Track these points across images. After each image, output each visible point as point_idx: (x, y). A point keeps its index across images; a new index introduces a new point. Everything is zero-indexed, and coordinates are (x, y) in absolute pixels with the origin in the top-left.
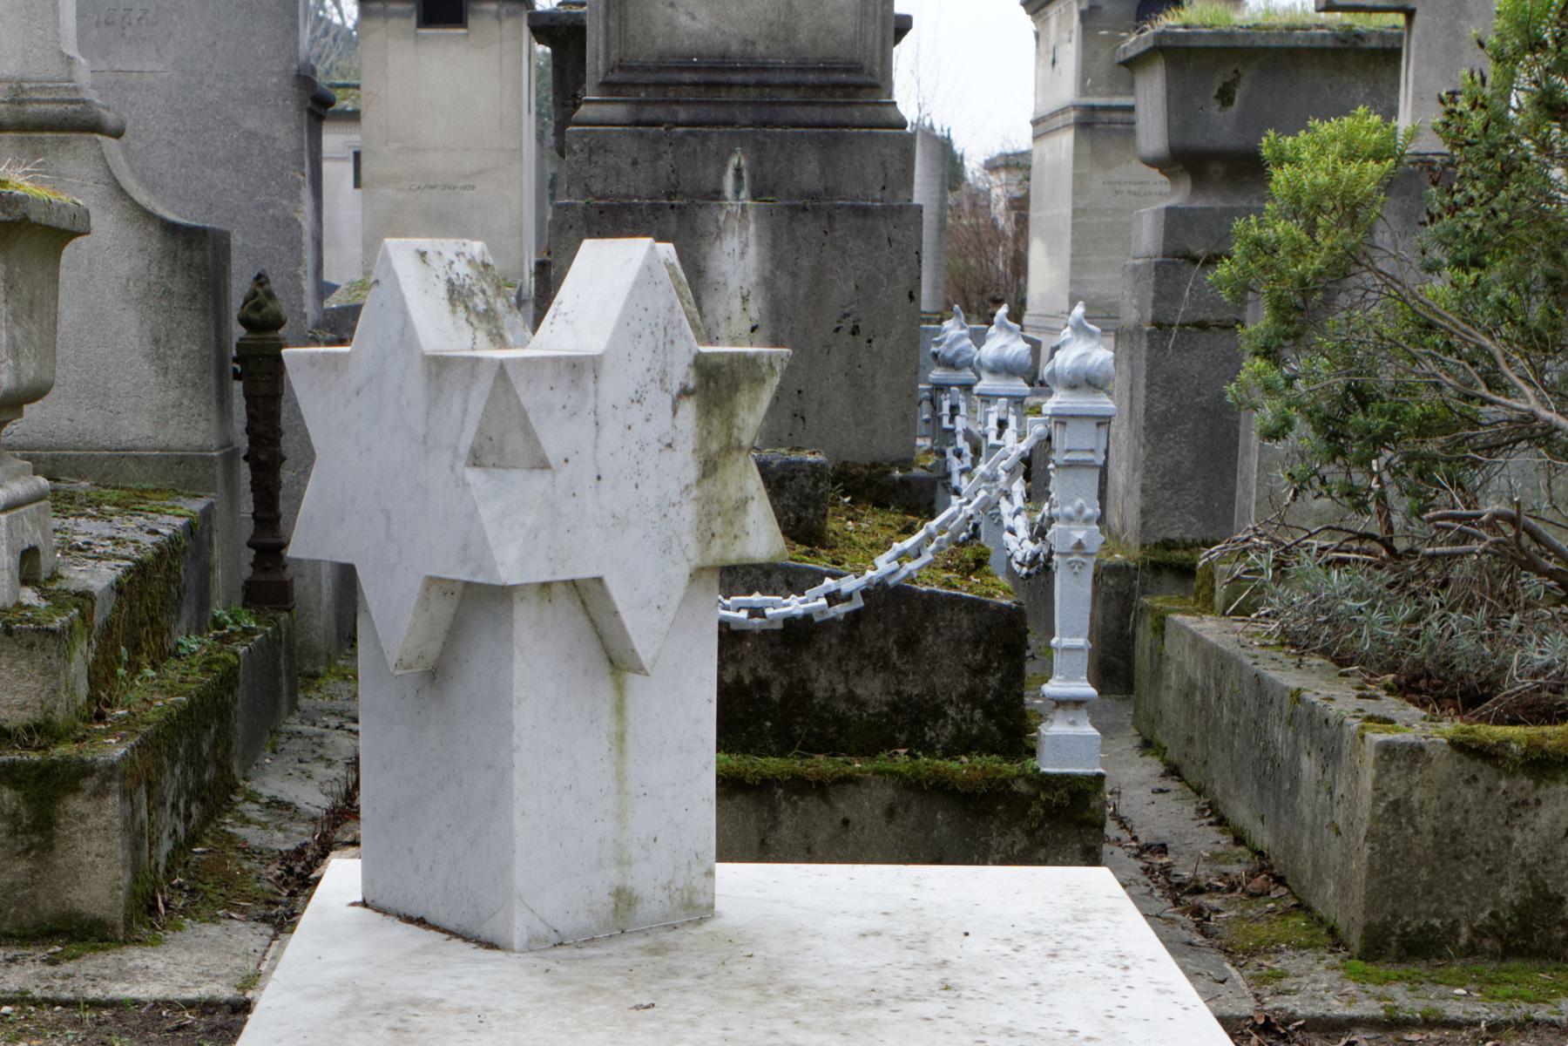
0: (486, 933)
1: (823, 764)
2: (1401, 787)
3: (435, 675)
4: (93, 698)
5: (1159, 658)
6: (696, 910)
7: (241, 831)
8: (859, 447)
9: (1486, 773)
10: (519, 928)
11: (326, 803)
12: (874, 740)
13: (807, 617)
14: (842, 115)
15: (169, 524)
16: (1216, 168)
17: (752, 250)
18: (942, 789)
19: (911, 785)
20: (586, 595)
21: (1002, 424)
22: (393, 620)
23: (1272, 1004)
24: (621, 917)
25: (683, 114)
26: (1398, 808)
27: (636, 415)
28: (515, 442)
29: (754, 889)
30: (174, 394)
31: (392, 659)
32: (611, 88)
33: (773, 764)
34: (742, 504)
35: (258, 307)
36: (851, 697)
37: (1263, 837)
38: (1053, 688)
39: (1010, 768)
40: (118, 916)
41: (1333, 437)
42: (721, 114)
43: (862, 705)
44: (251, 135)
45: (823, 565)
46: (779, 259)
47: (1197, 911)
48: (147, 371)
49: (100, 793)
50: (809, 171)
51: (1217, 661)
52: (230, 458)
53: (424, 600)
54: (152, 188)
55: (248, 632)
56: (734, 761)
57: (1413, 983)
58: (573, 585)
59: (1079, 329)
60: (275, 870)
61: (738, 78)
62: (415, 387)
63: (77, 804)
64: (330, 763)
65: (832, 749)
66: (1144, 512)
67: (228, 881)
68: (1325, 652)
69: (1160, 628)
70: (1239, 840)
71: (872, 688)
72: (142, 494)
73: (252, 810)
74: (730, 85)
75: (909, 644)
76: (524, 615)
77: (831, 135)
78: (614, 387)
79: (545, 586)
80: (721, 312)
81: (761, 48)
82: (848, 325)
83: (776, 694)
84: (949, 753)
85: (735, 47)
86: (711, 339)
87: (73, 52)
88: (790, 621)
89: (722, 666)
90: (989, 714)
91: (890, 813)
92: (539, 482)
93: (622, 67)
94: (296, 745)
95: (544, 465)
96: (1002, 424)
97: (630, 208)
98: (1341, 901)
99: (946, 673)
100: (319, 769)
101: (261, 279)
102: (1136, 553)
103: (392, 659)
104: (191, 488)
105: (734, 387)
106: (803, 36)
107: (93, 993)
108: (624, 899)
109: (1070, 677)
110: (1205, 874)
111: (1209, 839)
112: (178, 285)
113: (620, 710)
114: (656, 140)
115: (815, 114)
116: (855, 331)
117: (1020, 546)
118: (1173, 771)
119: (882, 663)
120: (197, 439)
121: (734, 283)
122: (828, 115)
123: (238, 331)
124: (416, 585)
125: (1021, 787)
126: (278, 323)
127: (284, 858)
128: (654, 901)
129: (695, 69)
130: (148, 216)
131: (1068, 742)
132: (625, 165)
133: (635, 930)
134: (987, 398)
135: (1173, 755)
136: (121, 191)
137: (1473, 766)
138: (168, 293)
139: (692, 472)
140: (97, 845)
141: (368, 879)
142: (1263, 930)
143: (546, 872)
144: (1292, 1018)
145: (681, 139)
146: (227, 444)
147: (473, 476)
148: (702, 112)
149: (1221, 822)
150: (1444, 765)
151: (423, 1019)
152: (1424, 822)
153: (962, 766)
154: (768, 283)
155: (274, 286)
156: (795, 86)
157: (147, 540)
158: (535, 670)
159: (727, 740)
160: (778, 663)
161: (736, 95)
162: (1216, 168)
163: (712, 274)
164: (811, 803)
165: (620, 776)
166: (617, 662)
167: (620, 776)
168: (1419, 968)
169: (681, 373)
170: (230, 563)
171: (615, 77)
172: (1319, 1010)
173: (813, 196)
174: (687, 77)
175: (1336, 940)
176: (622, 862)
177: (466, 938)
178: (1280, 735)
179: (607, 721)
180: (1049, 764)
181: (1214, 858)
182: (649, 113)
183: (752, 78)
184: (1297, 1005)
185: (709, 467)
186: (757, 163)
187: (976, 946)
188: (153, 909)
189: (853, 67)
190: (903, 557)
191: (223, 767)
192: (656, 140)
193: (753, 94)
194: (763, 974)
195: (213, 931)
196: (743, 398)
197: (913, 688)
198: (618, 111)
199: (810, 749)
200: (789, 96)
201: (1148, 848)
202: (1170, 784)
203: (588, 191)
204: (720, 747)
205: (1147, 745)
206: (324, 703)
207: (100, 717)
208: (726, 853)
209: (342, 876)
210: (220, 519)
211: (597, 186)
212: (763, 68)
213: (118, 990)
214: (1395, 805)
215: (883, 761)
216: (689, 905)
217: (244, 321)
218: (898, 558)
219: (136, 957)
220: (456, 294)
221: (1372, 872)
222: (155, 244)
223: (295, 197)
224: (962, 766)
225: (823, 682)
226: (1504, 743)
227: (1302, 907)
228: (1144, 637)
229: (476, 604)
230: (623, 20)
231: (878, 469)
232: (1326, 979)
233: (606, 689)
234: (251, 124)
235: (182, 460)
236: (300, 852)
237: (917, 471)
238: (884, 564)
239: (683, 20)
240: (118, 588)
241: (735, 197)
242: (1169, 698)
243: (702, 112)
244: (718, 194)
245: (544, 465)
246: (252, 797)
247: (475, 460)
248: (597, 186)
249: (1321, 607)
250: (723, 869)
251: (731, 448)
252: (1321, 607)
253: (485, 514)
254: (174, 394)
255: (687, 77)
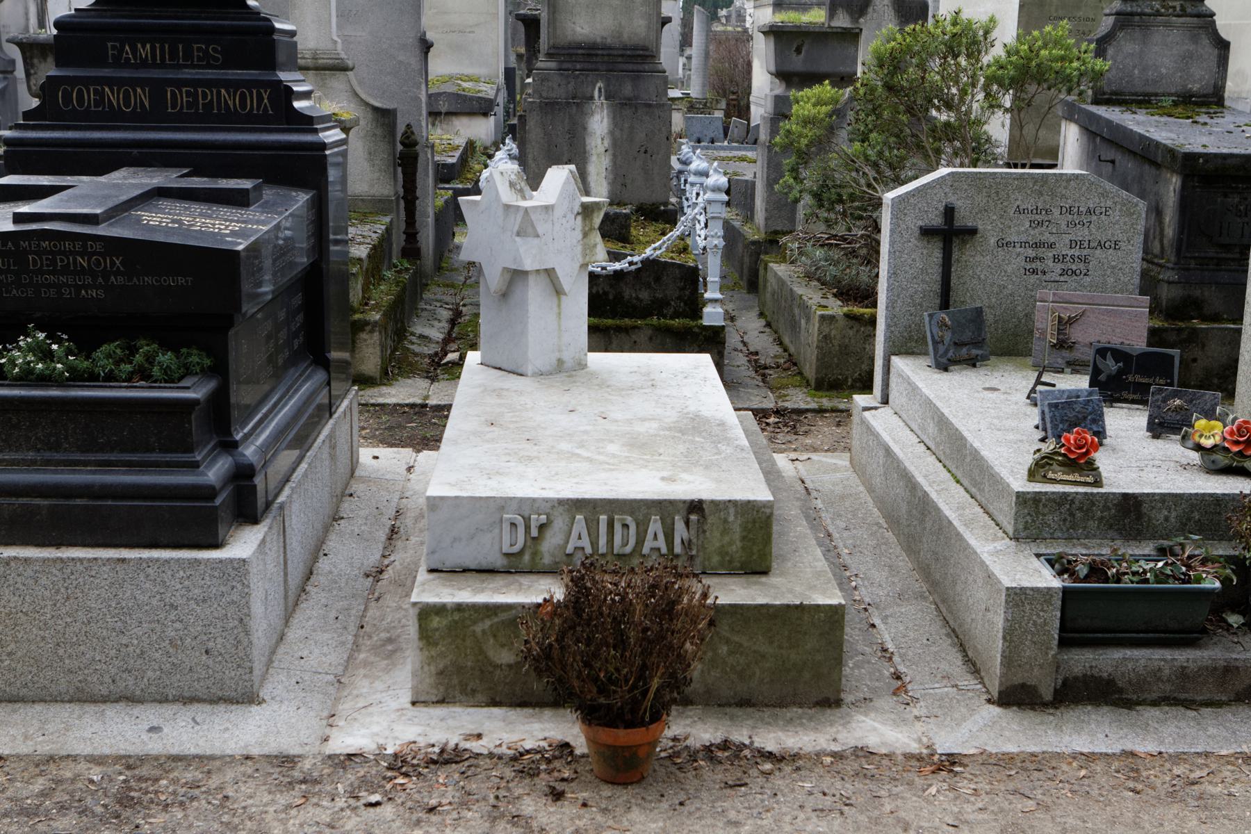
0: (520, 371)
1: (627, 321)
2: (827, 330)
3: (505, 295)
4: (364, 297)
5: (766, 281)
6: (582, 365)
7: (412, 347)
8: (647, 196)
9: (857, 326)
10: (530, 369)
11: (442, 336)
12: (645, 313)
13: (622, 270)
14: (640, 67)
15: (380, 229)
16: (796, 79)
17: (605, 120)
18: (668, 331)
19: (658, 329)
20: (550, 273)
21: (698, 194)
22: (493, 278)
23: (780, 404)
24: (559, 368)
25: (578, 67)
26: (826, 338)
27: (564, 221)
28: (530, 230)
29: (599, 360)
30: (377, 175)
31: (492, 290)
32: (550, 55)
33: (610, 322)
34: (595, 246)
35: (408, 138)
36: (637, 298)
37: (792, 349)
38: (707, 295)
39: (692, 323)
40: (378, 375)
41: (820, 200)
42: (593, 66)
43: (642, 301)
44: (400, 62)
45: (627, 252)
46: (616, 122)
47: (764, 375)
48: (366, 164)
49: (372, 332)
50: (627, 89)
51: (781, 282)
52: (397, 199)
53: (502, 274)
54: (360, 83)
55: (407, 269)
56: (596, 321)
57: (830, 398)
58: (546, 270)
59: (716, 170)
60: (427, 360)
61: (600, 52)
62: (500, 212)
63: (363, 335)
64: (440, 321)
65: (631, 317)
66: (766, 219)
67: (410, 364)
68: (819, 280)
69: (766, 269)
70: (785, 350)
71: (645, 295)
72: (365, 214)
73: (414, 339)
74: (597, 55)
75: (658, 279)
76: (531, 279)
77: (636, 76)
78: (558, 213)
79: (538, 271)
80: (593, 144)
81: (609, 41)
82: (643, 150)
83: (611, 297)
84: (672, 318)
85: (599, 40)
86: (587, 194)
87: (335, 38)
88: (615, 272)
89: (590, 288)
90: (686, 304)
91: (651, 339)
92: (536, 241)
93: (554, 47)
94: (425, 314)
95: (538, 236)
96: (698, 194)
97: (557, 103)
98: (810, 371)
99: (671, 290)
100: (436, 323)
101: (409, 126)
102: (763, 236)
103: (492, 290)
104: (384, 212)
105: (593, 211)
106: (625, 36)
107: (372, 401)
108: (560, 362)
109: (714, 292)
110: (769, 361)
111: (777, 350)
112: (379, 132)
113: (559, 306)
114: (568, 76)
115: (630, 67)
116: (646, 152)
117: (701, 243)
118: (768, 325)
119: (648, 286)
120: (386, 192)
121: (598, 133)
122: (635, 67)
123: (400, 147)
124: (500, 270)
125: (696, 330)
126: (416, 143)
127: (430, 356)
128: (569, 363)
129: (582, 48)
130: (367, 104)
131: (712, 315)
132: (555, 86)
133: (563, 371)
134: (693, 184)
135: (769, 319)
136: (357, 95)
137: (851, 323)
138: (375, 135)
139: (580, 236)
140: (371, 350)
141: (483, 357)
142: (785, 381)
143: (538, 351)
144: (786, 409)
145: (578, 76)
146: (396, 193)
147: (518, 239)
148: (586, 66)
149: (781, 344)
150: (842, 322)
151: (505, 393)
152: (836, 343)
153: (676, 322)
154: (611, 133)
155: (414, 129)
156: (622, 56)
157: (374, 236)
158: (535, 293)
159: (591, 313)
160: (611, 286)
161: (599, 59)
162: (796, 79)
163: (590, 129)
164: (623, 335)
165: (559, 326)
166: (558, 291)
167: (559, 326)
168: (834, 393)
169: (577, 208)
170: (398, 241)
171: (552, 51)
172: (796, 406)
173: (629, 99)
174: (580, 52)
175: (808, 384)
176: (560, 351)
177: (514, 373)
178: (796, 311)
179: (555, 309)
180: (706, 322)
181: (775, 356)
182: (565, 66)
183: (605, 52)
184: (789, 405)
185: (585, 235)
186: (607, 86)
187: (663, 375)
188: (387, 374)
189: (645, 48)
190: (655, 249)
191: (403, 322)
192: (568, 76)
193: (606, 59)
194: (601, 382)
195: (409, 381)
196: (595, 215)
197: (659, 295)
198: (553, 65)
199: (623, 317)
200: (620, 59)
201: (751, 353)
202: (767, 330)
203: (541, 96)
204: (589, 315)
205: (761, 315)
206: (432, 296)
207: (366, 304)
208: (590, 350)
209: (473, 357)
210: (395, 223)
211: (544, 94)
212: (610, 48)
213: (381, 400)
214: (825, 337)
215: (648, 321)
216: (580, 364)
217: (402, 143)
218: (656, 248)
219: (384, 389)
220: (512, 185)
221: (818, 359)
222: (370, 116)
223: (419, 88)
224: (676, 322)
225: (628, 293)
226: (862, 315)
227: (800, 373)
228: (761, 272)
229: (517, 276)
230: (555, 29)
231: (655, 206)
232: (801, 396)
233: (555, 299)
234: (401, 58)
235: (380, 201)
236: (436, 354)
237: (670, 207)
238: (648, 252)
239: (578, 29)
240: (369, 256)
241: (599, 100)
242: (768, 295)
243: (586, 66)
244: (592, 98)
245: (538, 236)
246: (413, 334)
247: (518, 234)
248: (544, 94)
249: (814, 263)
250: (590, 354)
251: (591, 229)
252: (814, 263)
253: (521, 250)
254: (377, 175)
255: (580, 52)
